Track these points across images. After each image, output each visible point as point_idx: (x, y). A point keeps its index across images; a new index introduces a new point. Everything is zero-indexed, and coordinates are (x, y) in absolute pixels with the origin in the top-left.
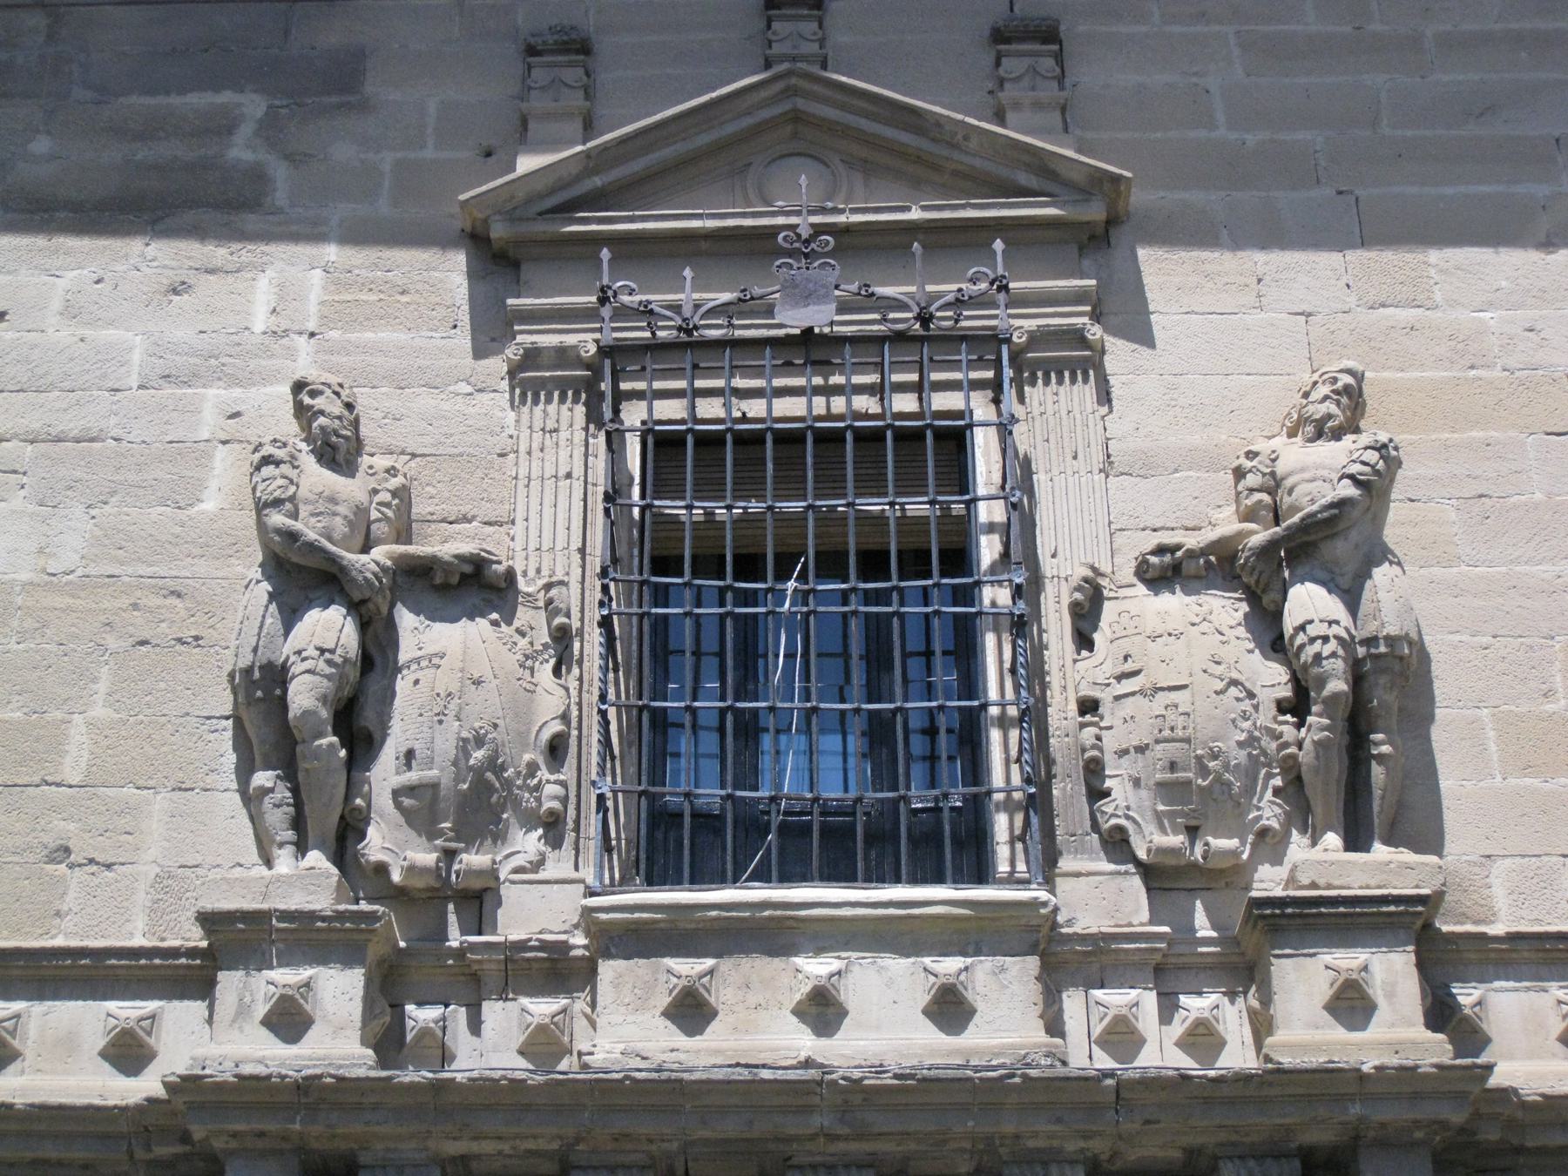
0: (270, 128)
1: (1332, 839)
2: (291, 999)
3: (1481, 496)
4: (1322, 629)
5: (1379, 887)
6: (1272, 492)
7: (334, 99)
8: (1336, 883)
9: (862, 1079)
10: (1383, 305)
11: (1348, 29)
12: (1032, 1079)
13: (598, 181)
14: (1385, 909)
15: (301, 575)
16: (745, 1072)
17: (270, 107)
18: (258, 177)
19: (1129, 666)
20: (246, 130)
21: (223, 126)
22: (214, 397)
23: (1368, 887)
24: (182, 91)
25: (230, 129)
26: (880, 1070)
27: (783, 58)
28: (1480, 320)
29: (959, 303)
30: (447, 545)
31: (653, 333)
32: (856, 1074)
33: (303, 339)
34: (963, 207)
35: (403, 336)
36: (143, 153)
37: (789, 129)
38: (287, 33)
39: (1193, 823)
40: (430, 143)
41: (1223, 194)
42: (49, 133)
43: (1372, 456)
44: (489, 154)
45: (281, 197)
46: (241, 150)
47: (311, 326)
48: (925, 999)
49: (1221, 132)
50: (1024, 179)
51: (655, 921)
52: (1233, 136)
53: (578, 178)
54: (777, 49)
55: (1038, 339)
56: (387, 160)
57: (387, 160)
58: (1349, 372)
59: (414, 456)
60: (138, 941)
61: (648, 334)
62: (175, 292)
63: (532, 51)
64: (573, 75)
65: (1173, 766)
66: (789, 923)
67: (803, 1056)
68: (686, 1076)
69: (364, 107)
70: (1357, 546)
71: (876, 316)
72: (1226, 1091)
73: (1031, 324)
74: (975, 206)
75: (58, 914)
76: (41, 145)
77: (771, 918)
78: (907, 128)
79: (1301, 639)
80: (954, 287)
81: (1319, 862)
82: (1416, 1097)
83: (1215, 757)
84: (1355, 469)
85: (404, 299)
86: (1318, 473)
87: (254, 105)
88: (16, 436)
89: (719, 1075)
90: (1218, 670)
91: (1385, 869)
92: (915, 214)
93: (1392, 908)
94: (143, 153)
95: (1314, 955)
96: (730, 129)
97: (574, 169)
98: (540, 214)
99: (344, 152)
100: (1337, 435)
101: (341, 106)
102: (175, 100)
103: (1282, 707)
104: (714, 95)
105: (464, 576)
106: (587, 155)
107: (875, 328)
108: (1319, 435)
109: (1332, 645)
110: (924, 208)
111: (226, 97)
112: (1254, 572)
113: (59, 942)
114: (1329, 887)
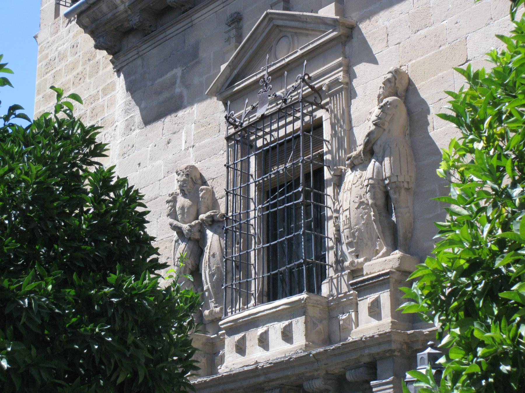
3: (440, 99)
5: (383, 270)
8: (372, 272)
9: (263, 366)
10: (418, 31)
13: (236, 72)
14: (381, 279)
16: (242, 369)
23: (380, 271)
28: (443, 24)
29: (248, 115)
31: (311, 87)
34: (309, 45)
35: (209, 140)
37: (277, 30)
38: (185, 42)
39: (357, 254)
41: (379, 3)
51: (232, 325)
55: (330, 86)
59: (213, 179)
61: (310, 90)
62: (169, 143)
66: (256, 319)
68: (232, 373)
70: (381, 146)
71: (274, 105)
72: (336, 352)
73: (327, 82)
74: (312, 43)
77: (242, 322)
78: (293, 21)
80: (291, 86)
82: (379, 344)
85: (210, 126)
89: (241, 370)
92: (300, 53)
93: (382, 278)
95: (367, 298)
96: (261, 38)
97: (228, 71)
98: (228, 87)
104: (251, 32)
106: (229, 66)
107: (275, 108)
110: (301, 49)
114: (371, 274)
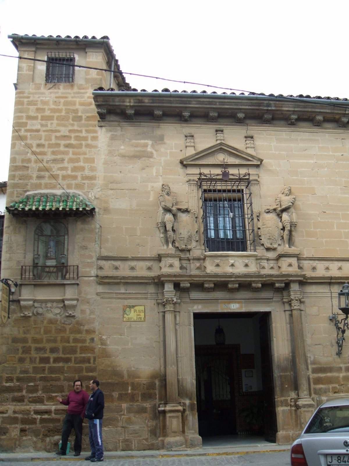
0: (153, 146)
1: (287, 246)
2: (172, 264)
4: (287, 221)
6: (280, 202)
7: (161, 142)
11: (289, 137)
12: (5, 417)
15: (167, 210)
17: (152, 143)
18: (152, 153)
19: (264, 224)
20: (149, 146)
21: (146, 146)
22: (150, 185)
24: (140, 140)
25: (147, 146)
26: (240, 274)
27: (219, 140)
30: (184, 207)
32: (237, 274)
33: (160, 177)
36: (136, 149)
40: (174, 149)
42: (123, 145)
43: (293, 200)
44: (181, 151)
45: (155, 156)
46: (149, 149)
47: (161, 175)
48: (244, 265)
49: (273, 152)
50: (250, 158)
52: (275, 152)
53: (194, 156)
54: (218, 138)
56: (168, 151)
57: (168, 151)
58: (290, 187)
60: (149, 256)
63: (186, 136)
64: (192, 141)
65: (269, 237)
67: (231, 272)
69: (165, 143)
75: (139, 252)
76: (122, 147)
79: (284, 222)
81: (285, 248)
83: (274, 236)
84: (291, 201)
86: (286, 201)
87: (150, 142)
88: (125, 189)
89: (222, 274)
90: (275, 225)
91: (293, 250)
94: (136, 149)
99: (163, 150)
100: (289, 195)
101: (161, 143)
102: (139, 141)
103: (282, 229)
105: (185, 211)
108: (286, 196)
109: (288, 223)
111: (146, 141)
112: (280, 212)
113: (139, 256)
